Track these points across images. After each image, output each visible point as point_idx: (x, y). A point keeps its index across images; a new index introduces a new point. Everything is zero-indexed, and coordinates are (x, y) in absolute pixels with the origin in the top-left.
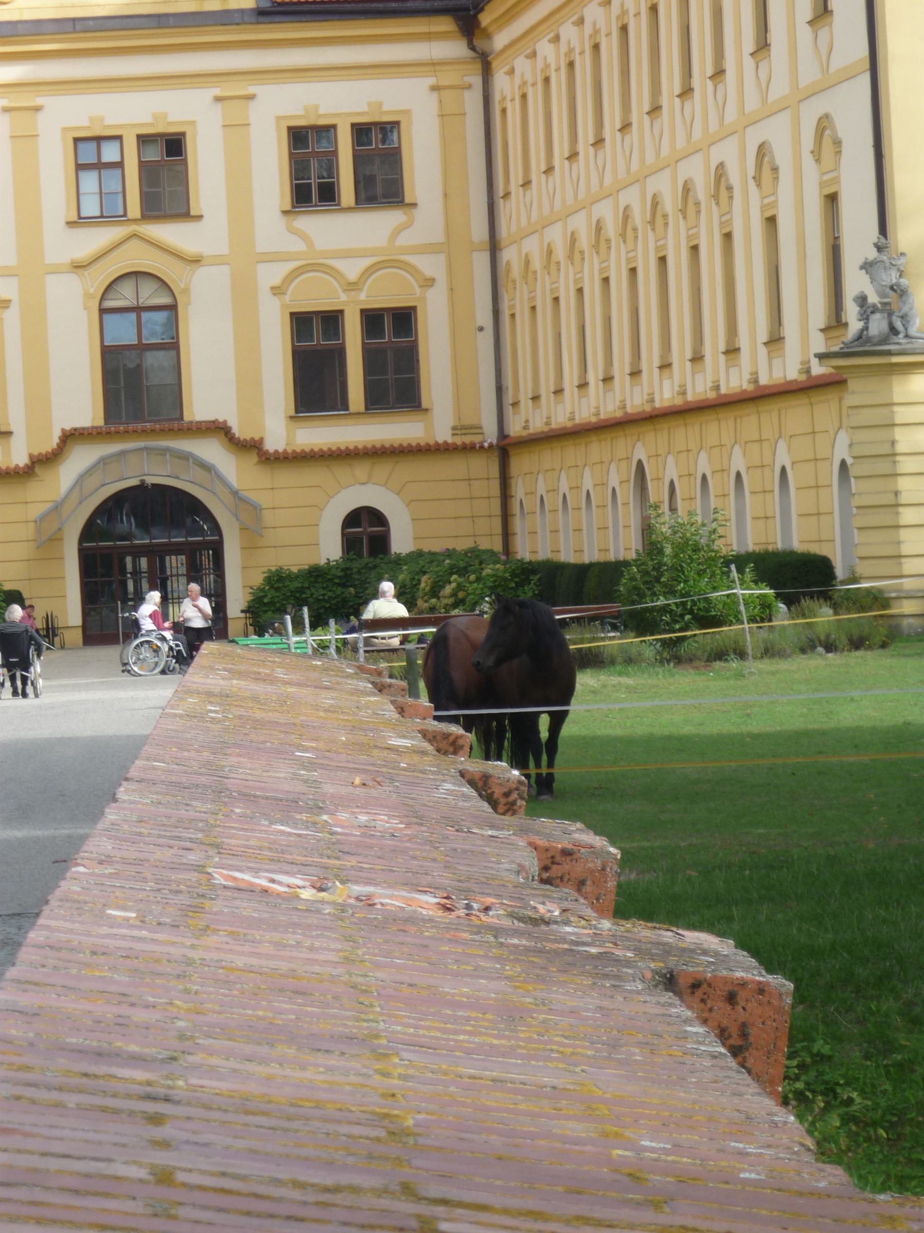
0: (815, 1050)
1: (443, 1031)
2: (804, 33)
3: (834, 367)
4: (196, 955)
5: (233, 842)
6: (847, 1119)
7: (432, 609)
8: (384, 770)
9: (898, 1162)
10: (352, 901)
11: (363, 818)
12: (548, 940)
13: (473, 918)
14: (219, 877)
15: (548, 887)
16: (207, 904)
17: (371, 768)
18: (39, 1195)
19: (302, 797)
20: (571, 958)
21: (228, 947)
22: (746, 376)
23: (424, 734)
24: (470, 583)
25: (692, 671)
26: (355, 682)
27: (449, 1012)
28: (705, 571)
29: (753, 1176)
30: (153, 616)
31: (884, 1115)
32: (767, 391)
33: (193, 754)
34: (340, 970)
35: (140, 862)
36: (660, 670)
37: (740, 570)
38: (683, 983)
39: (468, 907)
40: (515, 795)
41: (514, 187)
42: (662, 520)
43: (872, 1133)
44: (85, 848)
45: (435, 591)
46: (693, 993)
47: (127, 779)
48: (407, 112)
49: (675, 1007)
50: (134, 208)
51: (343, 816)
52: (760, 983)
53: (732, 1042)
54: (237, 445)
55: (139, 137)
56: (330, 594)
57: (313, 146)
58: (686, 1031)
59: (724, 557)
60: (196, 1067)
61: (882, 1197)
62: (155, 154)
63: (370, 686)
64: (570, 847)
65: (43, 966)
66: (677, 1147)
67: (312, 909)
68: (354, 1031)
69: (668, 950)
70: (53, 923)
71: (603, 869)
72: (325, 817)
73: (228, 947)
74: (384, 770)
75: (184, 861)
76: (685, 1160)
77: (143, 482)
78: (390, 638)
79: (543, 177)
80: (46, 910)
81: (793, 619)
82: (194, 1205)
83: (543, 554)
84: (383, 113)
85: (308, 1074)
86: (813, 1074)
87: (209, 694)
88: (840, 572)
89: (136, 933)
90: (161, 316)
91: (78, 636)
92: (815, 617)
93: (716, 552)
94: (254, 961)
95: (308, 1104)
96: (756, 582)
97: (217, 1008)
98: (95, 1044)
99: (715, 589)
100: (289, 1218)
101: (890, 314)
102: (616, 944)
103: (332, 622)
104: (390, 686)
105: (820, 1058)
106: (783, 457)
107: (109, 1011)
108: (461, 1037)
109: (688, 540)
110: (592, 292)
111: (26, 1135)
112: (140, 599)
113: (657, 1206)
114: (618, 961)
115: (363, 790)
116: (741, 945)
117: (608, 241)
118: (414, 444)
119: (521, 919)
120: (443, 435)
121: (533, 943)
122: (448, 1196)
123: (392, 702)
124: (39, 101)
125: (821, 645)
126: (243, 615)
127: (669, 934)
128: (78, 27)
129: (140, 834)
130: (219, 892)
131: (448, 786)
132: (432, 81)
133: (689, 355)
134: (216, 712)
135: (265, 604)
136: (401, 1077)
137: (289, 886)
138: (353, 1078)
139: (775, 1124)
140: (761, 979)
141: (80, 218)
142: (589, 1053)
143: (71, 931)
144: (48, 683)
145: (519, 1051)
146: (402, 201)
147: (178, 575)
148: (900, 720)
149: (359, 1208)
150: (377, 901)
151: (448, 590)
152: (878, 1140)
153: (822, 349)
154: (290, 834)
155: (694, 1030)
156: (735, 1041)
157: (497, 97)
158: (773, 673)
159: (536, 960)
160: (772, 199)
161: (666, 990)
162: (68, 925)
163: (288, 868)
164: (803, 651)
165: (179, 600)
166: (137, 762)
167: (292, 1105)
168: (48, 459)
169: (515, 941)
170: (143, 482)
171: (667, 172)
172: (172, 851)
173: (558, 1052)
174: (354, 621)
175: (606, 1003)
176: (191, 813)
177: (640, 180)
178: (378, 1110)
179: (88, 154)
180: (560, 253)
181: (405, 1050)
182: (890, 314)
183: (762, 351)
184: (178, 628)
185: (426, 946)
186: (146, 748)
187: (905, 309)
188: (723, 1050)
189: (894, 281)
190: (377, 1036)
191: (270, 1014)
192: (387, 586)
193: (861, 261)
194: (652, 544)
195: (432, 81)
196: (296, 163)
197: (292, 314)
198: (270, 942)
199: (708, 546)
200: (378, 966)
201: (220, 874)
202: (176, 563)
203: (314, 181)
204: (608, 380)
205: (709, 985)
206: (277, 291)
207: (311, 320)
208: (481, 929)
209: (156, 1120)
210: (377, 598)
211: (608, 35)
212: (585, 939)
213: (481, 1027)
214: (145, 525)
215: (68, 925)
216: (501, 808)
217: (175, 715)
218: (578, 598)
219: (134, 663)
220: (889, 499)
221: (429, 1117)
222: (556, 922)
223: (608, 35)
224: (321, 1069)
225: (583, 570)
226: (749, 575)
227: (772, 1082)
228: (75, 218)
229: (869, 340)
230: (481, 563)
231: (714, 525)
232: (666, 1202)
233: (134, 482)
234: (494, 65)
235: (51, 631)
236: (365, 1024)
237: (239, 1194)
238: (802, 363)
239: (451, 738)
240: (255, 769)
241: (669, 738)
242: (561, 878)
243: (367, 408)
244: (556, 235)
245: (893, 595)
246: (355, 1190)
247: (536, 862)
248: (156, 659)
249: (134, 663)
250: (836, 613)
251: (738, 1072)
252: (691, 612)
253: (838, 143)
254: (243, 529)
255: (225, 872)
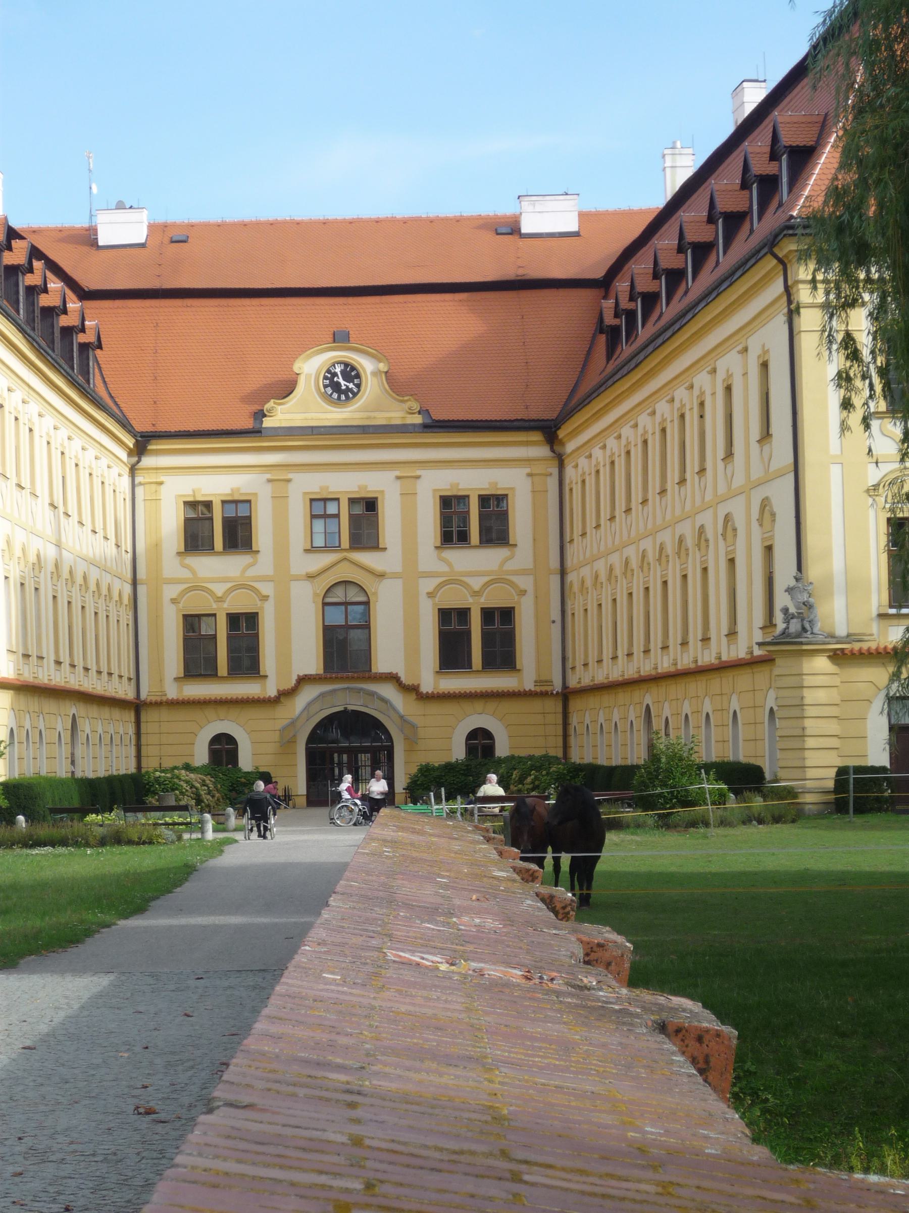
0: (746, 1068)
1: (527, 1055)
2: (755, 447)
3: (768, 651)
4: (374, 1003)
5: (399, 933)
6: (764, 1111)
7: (519, 791)
8: (490, 891)
9: (795, 1139)
10: (471, 972)
11: (477, 921)
12: (589, 1000)
13: (544, 985)
14: (390, 955)
15: (589, 967)
16: (383, 972)
17: (482, 889)
18: (280, 1150)
19: (441, 906)
20: (603, 1012)
21: (396, 999)
22: (714, 655)
23: (514, 869)
24: (543, 776)
25: (676, 834)
26: (473, 836)
27: (529, 1043)
28: (686, 772)
29: (713, 1151)
30: (348, 790)
31: (787, 1109)
32: (727, 665)
33: (374, 878)
34: (463, 1015)
35: (343, 944)
36: (656, 832)
37: (707, 773)
38: (671, 1029)
39: (541, 978)
40: (569, 909)
41: (576, 536)
42: (660, 741)
43: (780, 1120)
44: (310, 935)
45: (521, 780)
46: (676, 1035)
47: (335, 893)
48: (512, 489)
49: (666, 1044)
50: (345, 542)
51: (466, 919)
52: (717, 1030)
53: (699, 1066)
54: (404, 687)
55: (349, 499)
56: (457, 780)
57: (457, 508)
58: (673, 1060)
59: (697, 765)
60: (377, 1073)
61: (792, 1167)
62: (359, 510)
63: (482, 838)
64: (602, 942)
65: (284, 1008)
66: (667, 1131)
67: (447, 976)
68: (472, 1053)
69: (661, 1008)
70: (290, 981)
71: (622, 956)
72: (454, 919)
73: (396, 999)
74: (490, 891)
75: (369, 944)
76: (672, 1140)
77: (346, 708)
78: (494, 808)
79: (594, 530)
80: (286, 973)
81: (739, 803)
82: (375, 1160)
83: (588, 759)
84: (497, 489)
85: (445, 1080)
86: (744, 1083)
87: (385, 841)
88: (768, 776)
89: (340, 988)
90: (360, 608)
91: (303, 801)
92: (752, 803)
93: (693, 761)
94: (411, 1008)
95: (444, 1099)
96: (716, 780)
97: (389, 1036)
98: (315, 1057)
99: (691, 784)
100: (432, 1169)
101: (802, 620)
102: (630, 1004)
103: (459, 797)
104: (494, 838)
105: (749, 1073)
106: (735, 705)
107: (324, 1037)
108: (537, 1059)
109: (676, 754)
110: (622, 600)
111: (274, 1113)
112: (340, 781)
113: (654, 1168)
114: (631, 1015)
115: (477, 903)
116: (705, 1006)
117: (632, 570)
118: (511, 691)
119: (573, 986)
120: (529, 685)
121: (580, 1002)
122: (529, 1159)
123: (495, 848)
124: (290, 476)
125: (755, 820)
126: (404, 791)
127: (662, 998)
128: (314, 432)
129: (343, 927)
130: (391, 964)
131: (529, 902)
132: (528, 470)
133: (679, 641)
134: (388, 852)
135: (418, 785)
136: (500, 1083)
137: (432, 962)
138: (471, 1083)
139: (727, 1119)
140: (718, 1028)
141: (313, 547)
142: (614, 1071)
143: (299, 987)
144: (280, 829)
145: (572, 1069)
146: (508, 543)
147: (365, 766)
148: (803, 867)
149: (475, 1165)
150: (486, 973)
151: (529, 779)
152: (783, 1124)
153: (761, 640)
154: (433, 929)
155: (678, 1059)
156: (702, 1065)
157: (567, 481)
158: (726, 836)
159: (582, 1012)
160: (732, 548)
161: (660, 1033)
162: (299, 983)
163: (433, 950)
164: (744, 823)
165: (367, 781)
166: (341, 882)
167: (435, 1099)
168: (288, 693)
169: (569, 1000)
170: (346, 708)
171: (669, 530)
172: (362, 938)
173: (595, 1070)
174: (472, 797)
175: (624, 1041)
176: (373, 915)
177: (653, 533)
178: (486, 1103)
179: (318, 509)
180: (603, 577)
181: (502, 1066)
182: (802, 620)
183: (724, 640)
184: (365, 798)
185: (515, 1002)
186: (346, 873)
187: (812, 617)
188: (695, 1072)
189: (806, 599)
190: (486, 1057)
191: (421, 1042)
192: (493, 777)
193: (785, 587)
194: (654, 755)
195: (528, 470)
196: (444, 518)
197: (439, 609)
198: (421, 997)
199: (688, 757)
200: (486, 1013)
201: (391, 953)
202: (364, 759)
203: (455, 529)
204: (630, 655)
205: (687, 1031)
206: (430, 595)
207: (451, 613)
208: (549, 992)
209: (352, 1105)
210: (485, 784)
211: (636, 445)
212: (611, 1000)
213: (549, 1053)
214: (346, 735)
215: (299, 983)
216: (560, 916)
217: (364, 853)
218: (607, 787)
219: (338, 819)
220: (798, 732)
221: (517, 1109)
222: (594, 989)
223: (636, 445)
224: (452, 1077)
225: (611, 771)
226: (712, 776)
227: (723, 1092)
228: (309, 547)
229: (789, 635)
230: (549, 764)
231: (692, 745)
232: (660, 1166)
233: (341, 709)
234: (566, 462)
235: (287, 798)
236: (479, 1050)
237: (402, 1153)
238: (748, 648)
239: (531, 872)
240: (412, 888)
241: (661, 874)
242: (597, 961)
243: (483, 668)
244: (601, 566)
245: (800, 790)
246: (472, 1153)
247: (582, 950)
248: (351, 817)
249: (338, 819)
250: (765, 801)
251: (704, 1086)
252: (676, 797)
253: (773, 515)
254: (406, 739)
255: (394, 952)
